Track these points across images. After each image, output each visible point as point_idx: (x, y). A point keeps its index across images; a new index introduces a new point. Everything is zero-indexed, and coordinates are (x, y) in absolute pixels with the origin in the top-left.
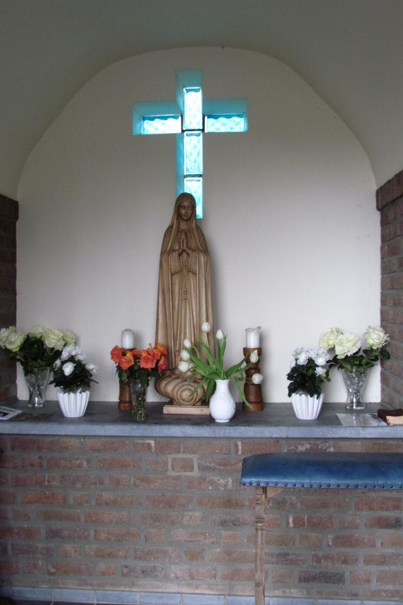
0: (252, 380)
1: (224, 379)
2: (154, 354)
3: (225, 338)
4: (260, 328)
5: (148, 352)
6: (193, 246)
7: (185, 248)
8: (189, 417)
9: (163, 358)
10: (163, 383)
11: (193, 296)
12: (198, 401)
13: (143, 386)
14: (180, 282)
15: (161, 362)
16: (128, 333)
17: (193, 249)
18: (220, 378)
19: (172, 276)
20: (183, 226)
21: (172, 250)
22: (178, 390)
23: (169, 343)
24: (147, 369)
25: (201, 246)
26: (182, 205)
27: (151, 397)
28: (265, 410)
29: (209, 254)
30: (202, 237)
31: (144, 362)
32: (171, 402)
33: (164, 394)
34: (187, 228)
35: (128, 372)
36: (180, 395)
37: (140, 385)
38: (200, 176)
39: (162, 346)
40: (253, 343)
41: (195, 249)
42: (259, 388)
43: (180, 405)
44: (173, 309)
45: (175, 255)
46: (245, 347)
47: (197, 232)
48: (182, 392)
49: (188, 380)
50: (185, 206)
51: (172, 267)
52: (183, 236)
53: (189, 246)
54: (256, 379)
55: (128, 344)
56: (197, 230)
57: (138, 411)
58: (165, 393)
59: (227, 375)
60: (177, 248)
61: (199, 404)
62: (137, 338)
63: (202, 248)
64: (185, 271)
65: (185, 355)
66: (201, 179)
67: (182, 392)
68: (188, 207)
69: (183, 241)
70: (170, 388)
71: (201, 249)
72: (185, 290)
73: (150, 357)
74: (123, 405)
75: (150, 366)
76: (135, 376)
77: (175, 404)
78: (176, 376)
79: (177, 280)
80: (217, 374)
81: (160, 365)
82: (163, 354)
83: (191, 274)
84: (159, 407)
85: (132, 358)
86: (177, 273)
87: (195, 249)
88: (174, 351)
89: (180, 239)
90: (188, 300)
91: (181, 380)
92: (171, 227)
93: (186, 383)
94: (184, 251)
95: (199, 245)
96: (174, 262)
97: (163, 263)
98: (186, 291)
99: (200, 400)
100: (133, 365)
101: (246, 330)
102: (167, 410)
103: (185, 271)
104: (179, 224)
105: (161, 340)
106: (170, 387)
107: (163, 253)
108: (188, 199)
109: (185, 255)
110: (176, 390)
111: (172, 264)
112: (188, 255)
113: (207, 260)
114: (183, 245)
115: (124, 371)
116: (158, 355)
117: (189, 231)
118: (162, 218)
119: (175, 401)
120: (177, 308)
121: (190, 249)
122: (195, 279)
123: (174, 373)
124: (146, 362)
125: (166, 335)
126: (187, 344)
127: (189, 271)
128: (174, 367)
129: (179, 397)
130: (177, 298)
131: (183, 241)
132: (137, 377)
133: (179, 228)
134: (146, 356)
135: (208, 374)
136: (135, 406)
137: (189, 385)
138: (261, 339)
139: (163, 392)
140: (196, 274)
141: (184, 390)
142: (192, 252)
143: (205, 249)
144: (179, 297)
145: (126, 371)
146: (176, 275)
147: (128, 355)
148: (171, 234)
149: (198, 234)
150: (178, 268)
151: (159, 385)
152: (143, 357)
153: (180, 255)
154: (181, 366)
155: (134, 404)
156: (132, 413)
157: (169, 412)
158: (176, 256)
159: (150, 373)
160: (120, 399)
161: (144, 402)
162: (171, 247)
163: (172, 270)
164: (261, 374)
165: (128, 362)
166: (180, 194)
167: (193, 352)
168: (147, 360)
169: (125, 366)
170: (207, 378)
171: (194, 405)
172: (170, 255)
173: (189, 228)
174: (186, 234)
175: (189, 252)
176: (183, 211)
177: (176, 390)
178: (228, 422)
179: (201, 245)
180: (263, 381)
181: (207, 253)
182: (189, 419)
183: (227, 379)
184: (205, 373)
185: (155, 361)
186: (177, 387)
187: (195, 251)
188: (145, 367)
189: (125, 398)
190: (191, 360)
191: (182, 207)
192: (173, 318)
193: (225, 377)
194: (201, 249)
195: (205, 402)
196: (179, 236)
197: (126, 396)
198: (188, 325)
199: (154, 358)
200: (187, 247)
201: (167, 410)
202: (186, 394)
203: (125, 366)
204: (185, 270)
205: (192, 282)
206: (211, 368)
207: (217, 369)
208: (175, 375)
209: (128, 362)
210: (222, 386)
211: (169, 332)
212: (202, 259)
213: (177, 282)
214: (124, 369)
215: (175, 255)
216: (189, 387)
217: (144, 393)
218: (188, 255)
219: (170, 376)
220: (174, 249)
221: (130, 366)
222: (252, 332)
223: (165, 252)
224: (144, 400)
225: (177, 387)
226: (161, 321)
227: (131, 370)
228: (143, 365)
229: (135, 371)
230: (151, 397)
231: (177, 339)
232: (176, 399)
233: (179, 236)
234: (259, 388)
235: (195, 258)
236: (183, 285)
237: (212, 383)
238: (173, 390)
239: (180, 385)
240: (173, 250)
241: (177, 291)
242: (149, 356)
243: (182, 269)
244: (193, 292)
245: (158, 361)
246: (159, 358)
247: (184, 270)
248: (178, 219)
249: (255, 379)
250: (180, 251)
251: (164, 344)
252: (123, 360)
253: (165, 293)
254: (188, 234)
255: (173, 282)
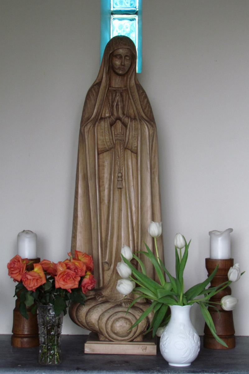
0: (221, 306)
1: (184, 305)
2: (76, 268)
3: (187, 246)
4: (231, 230)
5: (66, 265)
6: (131, 111)
7: (121, 116)
8: (126, 359)
9: (89, 273)
10: (84, 309)
11: (132, 184)
12: (138, 336)
13: (57, 315)
14: (111, 164)
15: (86, 280)
16: (28, 236)
17: (133, 117)
18: (177, 302)
19: (98, 154)
20: (117, 83)
21: (100, 118)
22: (108, 319)
23: (95, 252)
24: (66, 291)
25: (144, 113)
26: (116, 53)
27: (67, 329)
28: (237, 347)
29: (154, 123)
30: (146, 100)
31: (61, 280)
32: (96, 336)
33: (85, 324)
34: (123, 86)
35: (34, 294)
36: (112, 326)
37: (52, 313)
38: (136, 13)
39: (86, 255)
40: (220, 252)
41: (135, 116)
42: (229, 315)
43: (110, 340)
44: (100, 203)
45: (104, 125)
46: (208, 257)
47: (138, 94)
48: (114, 322)
49: (123, 304)
50: (120, 55)
51: (100, 142)
52: (118, 98)
53: (125, 112)
54: (227, 303)
55: (27, 251)
56: (138, 91)
57: (49, 350)
58: (87, 323)
59: (188, 298)
60: (107, 115)
61: (139, 339)
62: (40, 243)
63: (146, 115)
64: (119, 149)
65: (124, 270)
66: (136, 17)
67: (114, 322)
68: (126, 56)
69: (117, 105)
70: (94, 317)
71: (144, 117)
72: (120, 175)
73: (72, 272)
74: (18, 342)
75: (70, 285)
76: (46, 300)
77: (102, 338)
78: (104, 299)
79: (106, 160)
80: (174, 297)
81: (86, 284)
82: (89, 269)
83: (130, 152)
84: (78, 342)
85: (42, 274)
86: (108, 151)
87: (135, 116)
88: (102, 263)
89: (113, 102)
90: (123, 190)
91: (111, 305)
92: (96, 85)
93: (120, 309)
94: (119, 119)
95: (141, 111)
96: (103, 134)
97: (86, 137)
98: (122, 176)
99: (141, 333)
100: (44, 284)
101: (210, 233)
102: (91, 348)
103: (119, 149)
104: (110, 80)
105: (81, 245)
106: (95, 315)
107: (84, 122)
108: (125, 45)
109: (119, 125)
110: (105, 319)
111: (99, 137)
112: (125, 125)
113: (154, 133)
114: (118, 111)
115: (29, 293)
116: (82, 270)
117: (127, 90)
118: (80, 74)
119: (98, 332)
120: (106, 201)
121: (128, 116)
122: (134, 160)
123: (100, 295)
124: (64, 280)
125: (90, 240)
126: (127, 253)
127: (126, 148)
128: (101, 285)
129: (109, 330)
130: (106, 186)
131: (117, 105)
132: (48, 301)
133: (110, 85)
134: (65, 272)
135: (160, 297)
136: (44, 343)
137: (127, 312)
138: (233, 245)
139: (84, 321)
140: (137, 153)
141: (117, 320)
142: (131, 121)
143: (149, 118)
144: (110, 185)
145: (32, 292)
146: (105, 154)
147: (36, 269)
148: (97, 95)
149: (139, 96)
150: (109, 144)
151: (76, 313)
152: (59, 273)
153: (112, 125)
154: (121, 286)
155: (43, 340)
156: (39, 353)
157: (93, 350)
158: (106, 126)
159: (69, 295)
160: (13, 331)
161: (58, 337)
162: (98, 114)
163: (100, 147)
164: (233, 297)
165: (37, 279)
166: (108, 40)
167: (133, 263)
168: (66, 277)
169: (32, 285)
170: (158, 303)
171: (132, 341)
172: (96, 125)
173: (126, 86)
174: (122, 96)
175: (126, 120)
176: (117, 62)
177: (105, 319)
178: (190, 366)
179: (143, 111)
180: (237, 306)
181: (152, 123)
182: (127, 362)
183: (188, 304)
184: (156, 295)
185: (79, 279)
186: (107, 316)
187: (135, 119)
188: (62, 287)
189: (23, 331)
190: (133, 277)
191: (116, 56)
192: (100, 216)
193: (185, 302)
194: (144, 117)
195: (151, 335)
196: (110, 98)
197: (24, 328)
198: (123, 225)
199: (77, 274)
200: (123, 114)
201: (91, 348)
202: (121, 326)
203: (32, 285)
204: (121, 147)
205: (130, 164)
206: (163, 288)
207: (172, 290)
208: (102, 297)
209: (37, 279)
210: (180, 315)
211: (94, 236)
212: (146, 131)
213: (107, 164)
214: (29, 289)
215: (104, 125)
216: (130, 317)
217: (59, 325)
218: (125, 125)
219: (94, 299)
220: (103, 116)
221: (39, 285)
222: (219, 236)
223: (88, 120)
224: (58, 335)
225: (107, 316)
226: (80, 219)
227: (40, 291)
228: (60, 284)
229: (45, 292)
230: (67, 329)
231: (106, 247)
232: (104, 331)
233: (110, 98)
234: (229, 315)
235: (136, 129)
236: (117, 168)
237: (164, 310)
238: (100, 318)
239: (111, 312)
240: (101, 118)
241: (106, 175)
242: (68, 270)
243: (115, 144)
244: (131, 178)
245: (82, 278)
246: (84, 274)
247: (118, 147)
248: (108, 73)
249: (225, 303)
250: (113, 118)
251: (87, 253)
252: (29, 277)
253: (86, 179)
254: (124, 94)
255: (100, 163)
